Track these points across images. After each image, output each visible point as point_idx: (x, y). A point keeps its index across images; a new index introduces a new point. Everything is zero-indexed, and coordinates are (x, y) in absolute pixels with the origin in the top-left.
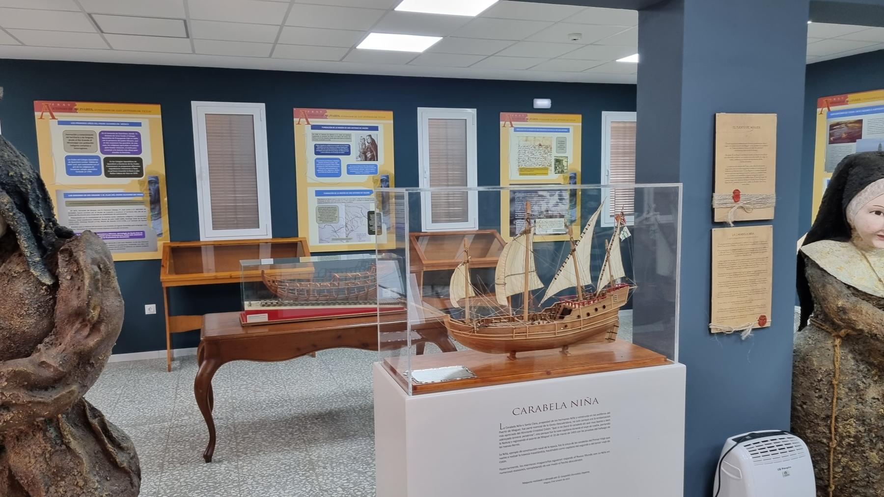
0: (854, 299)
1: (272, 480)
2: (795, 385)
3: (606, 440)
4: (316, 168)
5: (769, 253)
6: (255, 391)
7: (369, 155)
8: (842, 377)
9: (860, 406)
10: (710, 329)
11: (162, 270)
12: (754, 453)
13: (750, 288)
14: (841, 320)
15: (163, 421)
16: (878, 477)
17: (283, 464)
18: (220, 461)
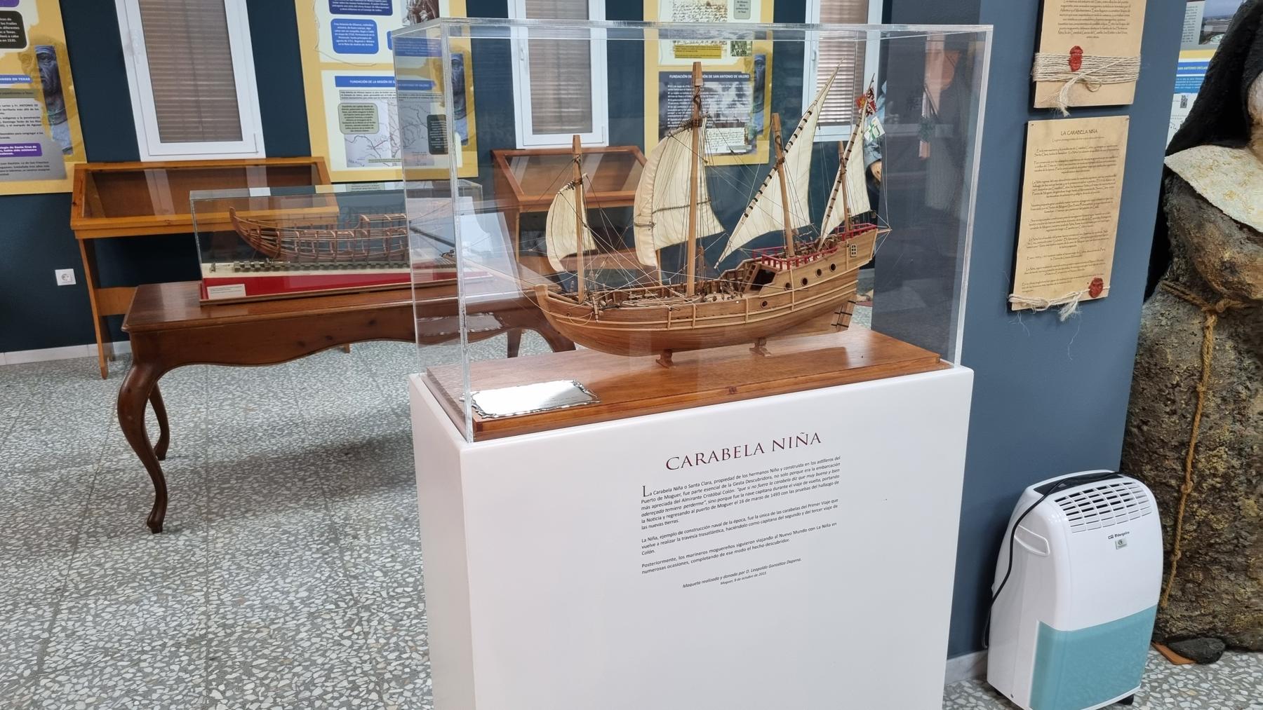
0: (1250, 247)
1: (265, 561)
2: (1135, 393)
3: (831, 505)
4: (335, 38)
5: (1119, 168)
6: (246, 410)
7: (424, 15)
8: (1213, 380)
9: (1238, 426)
10: (1009, 305)
11: (74, 210)
12: (1071, 512)
13: (1082, 231)
14: (1224, 284)
15: (86, 463)
16: (1254, 538)
17: (285, 532)
18: (177, 531)
